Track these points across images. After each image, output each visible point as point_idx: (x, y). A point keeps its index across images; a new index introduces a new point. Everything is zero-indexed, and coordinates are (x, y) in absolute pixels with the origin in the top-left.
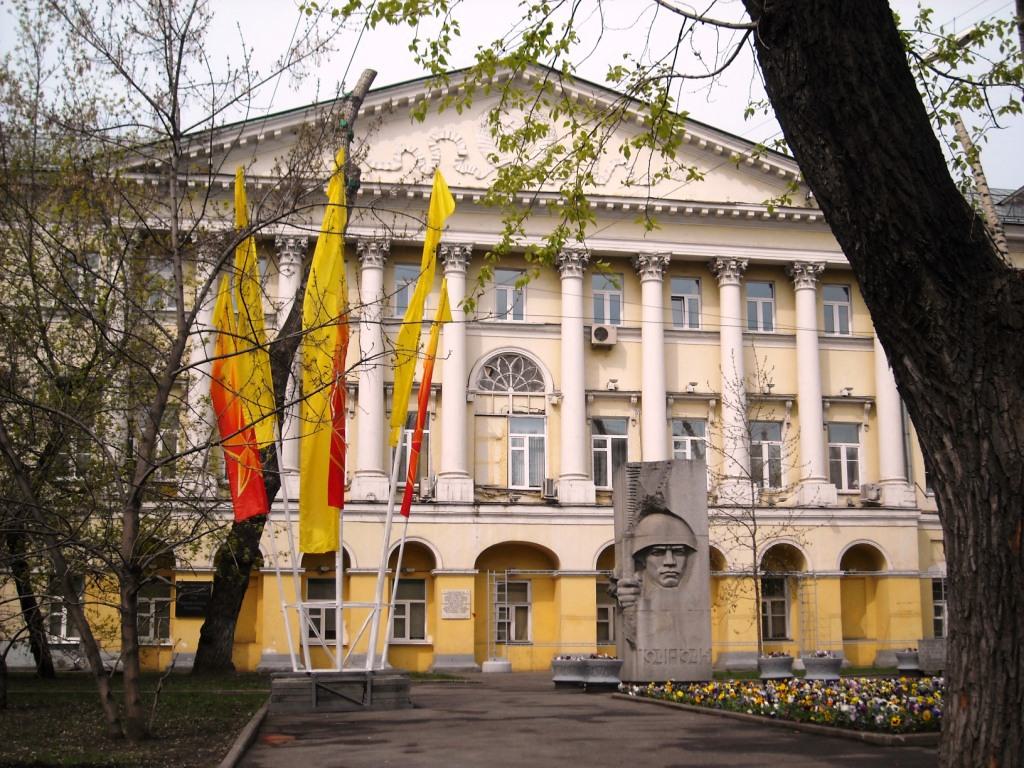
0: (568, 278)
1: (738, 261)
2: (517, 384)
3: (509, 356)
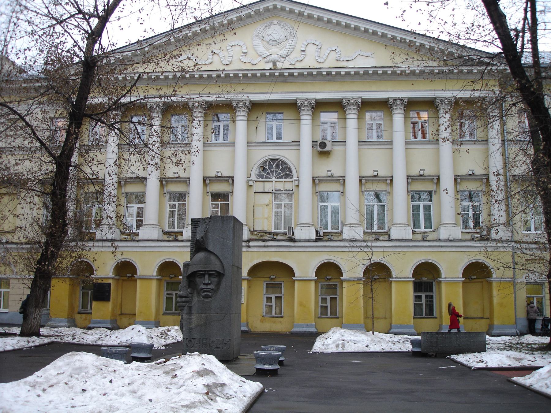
0: (304, 115)
1: (401, 99)
2: (278, 175)
3: (274, 160)
